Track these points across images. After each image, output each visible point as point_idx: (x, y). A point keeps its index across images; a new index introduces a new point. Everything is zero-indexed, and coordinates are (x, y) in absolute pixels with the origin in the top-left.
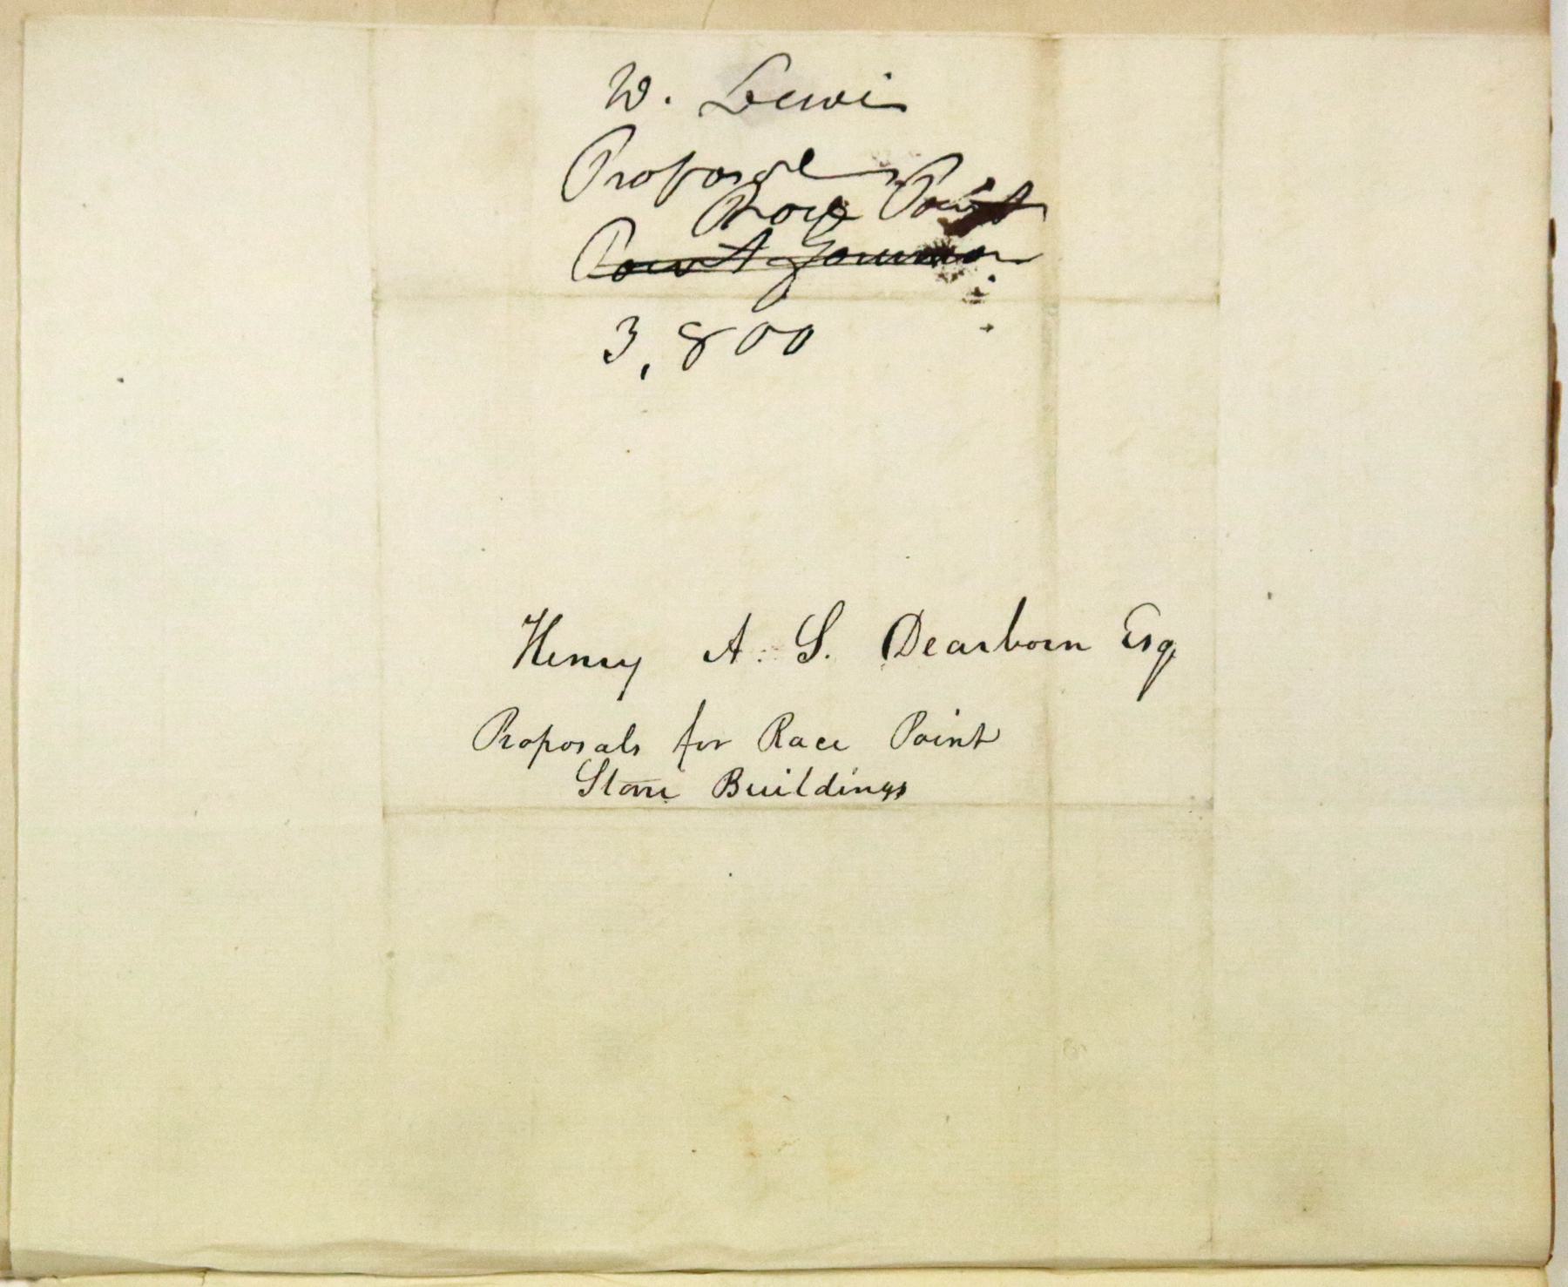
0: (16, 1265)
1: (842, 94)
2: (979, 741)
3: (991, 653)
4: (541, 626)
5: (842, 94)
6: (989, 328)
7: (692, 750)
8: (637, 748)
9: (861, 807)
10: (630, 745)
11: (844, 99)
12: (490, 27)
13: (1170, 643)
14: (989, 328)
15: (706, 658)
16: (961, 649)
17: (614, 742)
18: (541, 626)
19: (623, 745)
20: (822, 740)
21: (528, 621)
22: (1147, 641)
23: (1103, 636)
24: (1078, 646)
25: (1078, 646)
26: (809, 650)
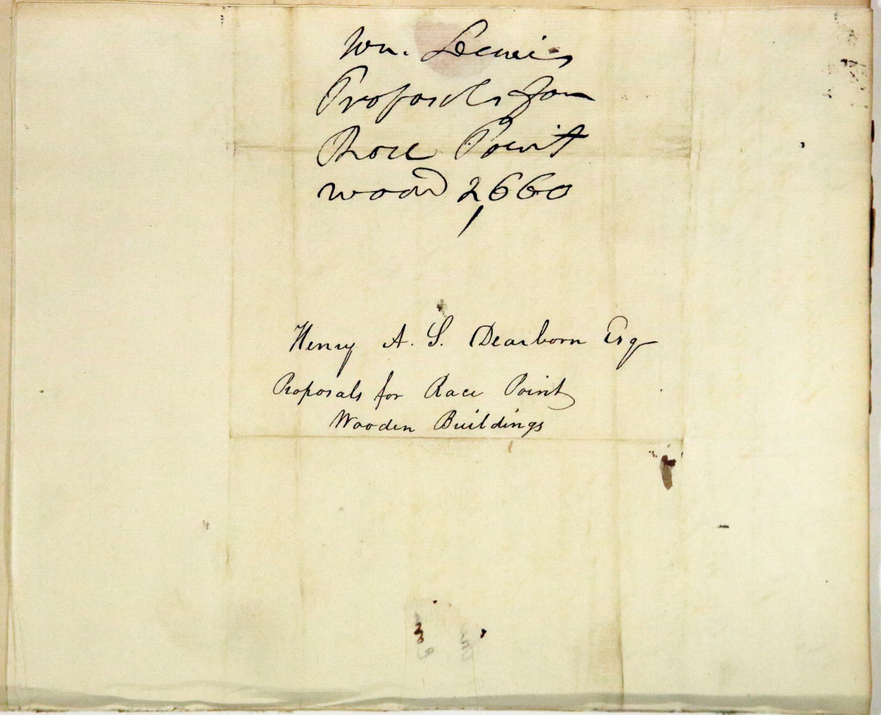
0: (11, 697)
1: (533, 52)
2: (558, 392)
3: (530, 346)
4: (305, 331)
5: (533, 52)
6: (803, 144)
7: (384, 399)
8: (360, 396)
9: (473, 439)
10: (356, 394)
11: (533, 55)
12: (431, 70)
13: (455, 411)
14: (803, 144)
15: (384, 346)
16: (512, 343)
17: (347, 393)
18: (305, 331)
19: (351, 394)
20: (466, 391)
21: (298, 326)
22: (620, 340)
23: (594, 334)
24: (578, 342)
25: (578, 342)
26: (434, 340)
